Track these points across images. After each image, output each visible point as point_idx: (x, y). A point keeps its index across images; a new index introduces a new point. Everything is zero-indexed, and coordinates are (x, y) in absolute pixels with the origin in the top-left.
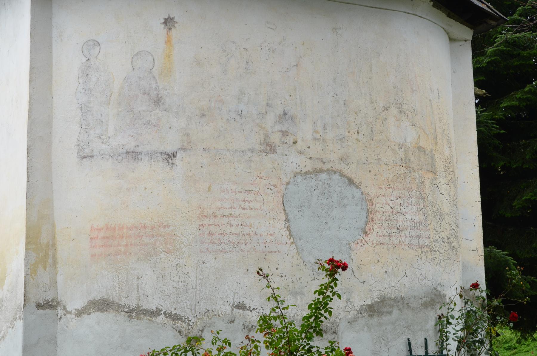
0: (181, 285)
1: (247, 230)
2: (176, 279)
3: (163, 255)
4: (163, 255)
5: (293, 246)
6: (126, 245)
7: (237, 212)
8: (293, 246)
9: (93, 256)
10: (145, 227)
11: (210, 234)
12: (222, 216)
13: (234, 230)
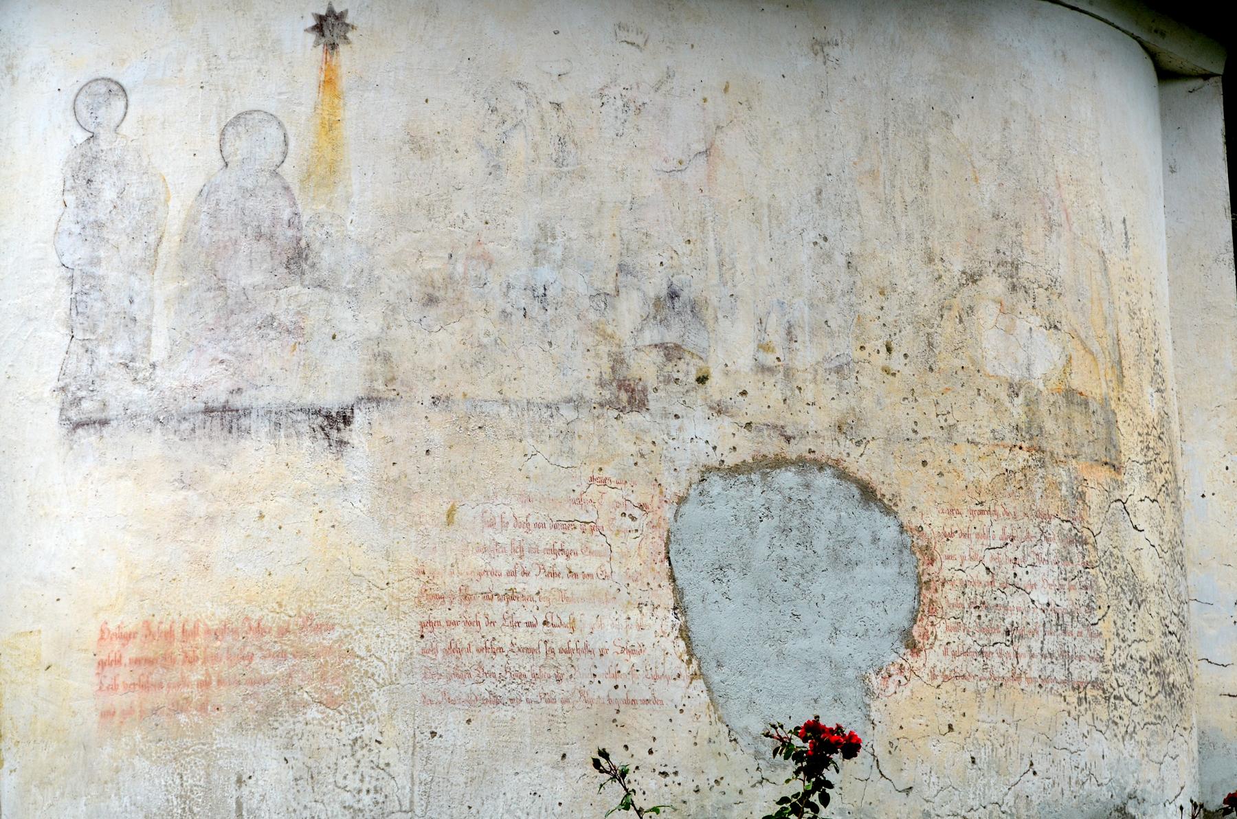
0: (367, 799)
1: (561, 637)
2: (353, 783)
3: (313, 713)
4: (313, 713)
5: (699, 683)
6: (205, 684)
7: (533, 584)
8: (699, 683)
9: (107, 714)
10: (260, 630)
11: (454, 649)
12: (488, 596)
13: (523, 637)
